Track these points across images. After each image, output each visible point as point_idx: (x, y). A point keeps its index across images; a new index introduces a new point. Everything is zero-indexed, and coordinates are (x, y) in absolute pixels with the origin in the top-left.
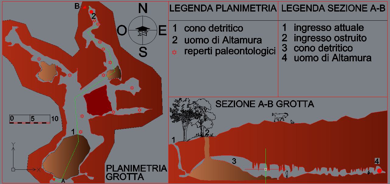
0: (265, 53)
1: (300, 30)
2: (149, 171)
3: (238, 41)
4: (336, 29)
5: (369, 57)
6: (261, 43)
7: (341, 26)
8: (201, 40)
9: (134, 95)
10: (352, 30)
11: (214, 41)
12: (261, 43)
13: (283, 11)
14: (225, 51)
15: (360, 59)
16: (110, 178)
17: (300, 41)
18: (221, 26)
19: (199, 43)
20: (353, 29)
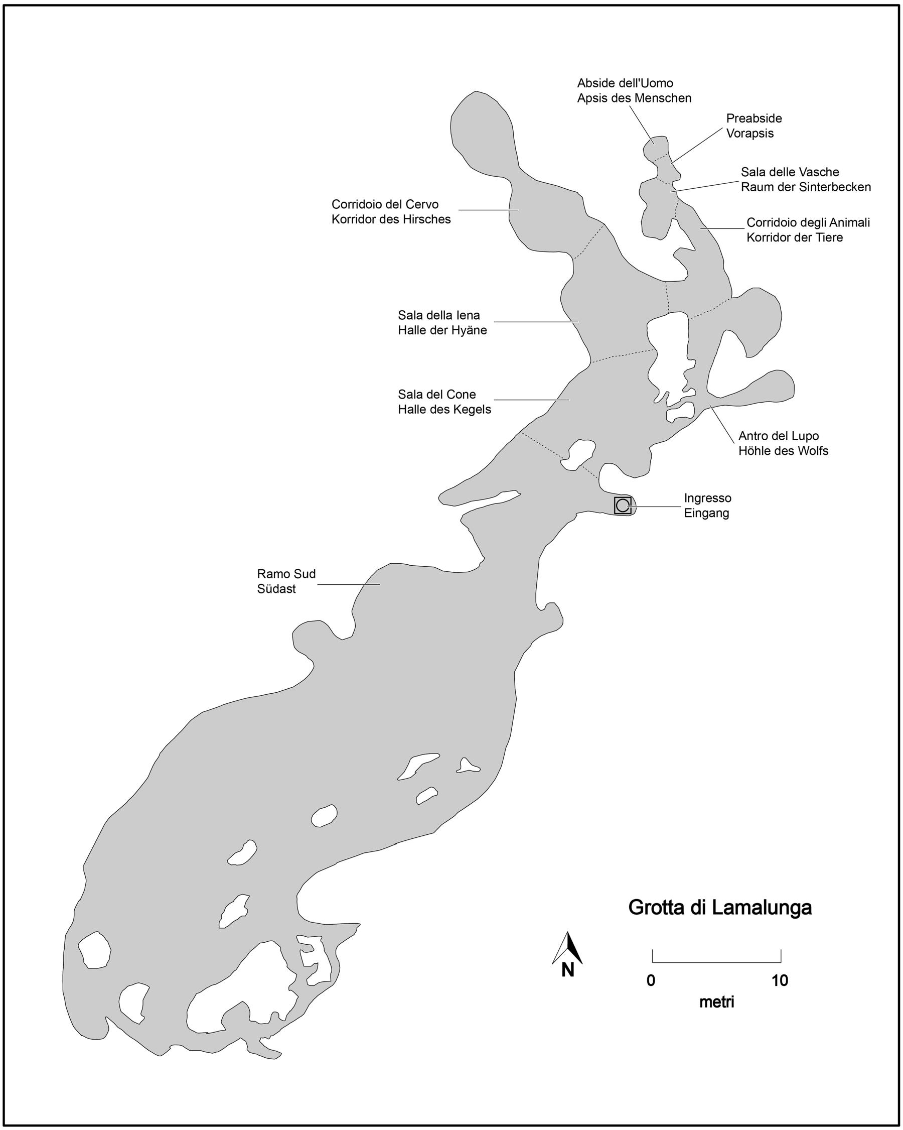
0: (798, 912)
1: (788, 913)
2: (714, 901)
3: (732, 908)
4: (728, 911)
5: (679, 906)
6: (810, 913)
7: (665, 904)
8: (709, 1002)
9: (729, 337)
10: (754, 913)
11: (696, 909)
12: (810, 913)
13: (715, 913)
14: (760, 908)
15: (773, 910)
16: (639, 910)
17: (788, 913)
18: (723, 999)
19: (743, 913)
20: (756, 911)
